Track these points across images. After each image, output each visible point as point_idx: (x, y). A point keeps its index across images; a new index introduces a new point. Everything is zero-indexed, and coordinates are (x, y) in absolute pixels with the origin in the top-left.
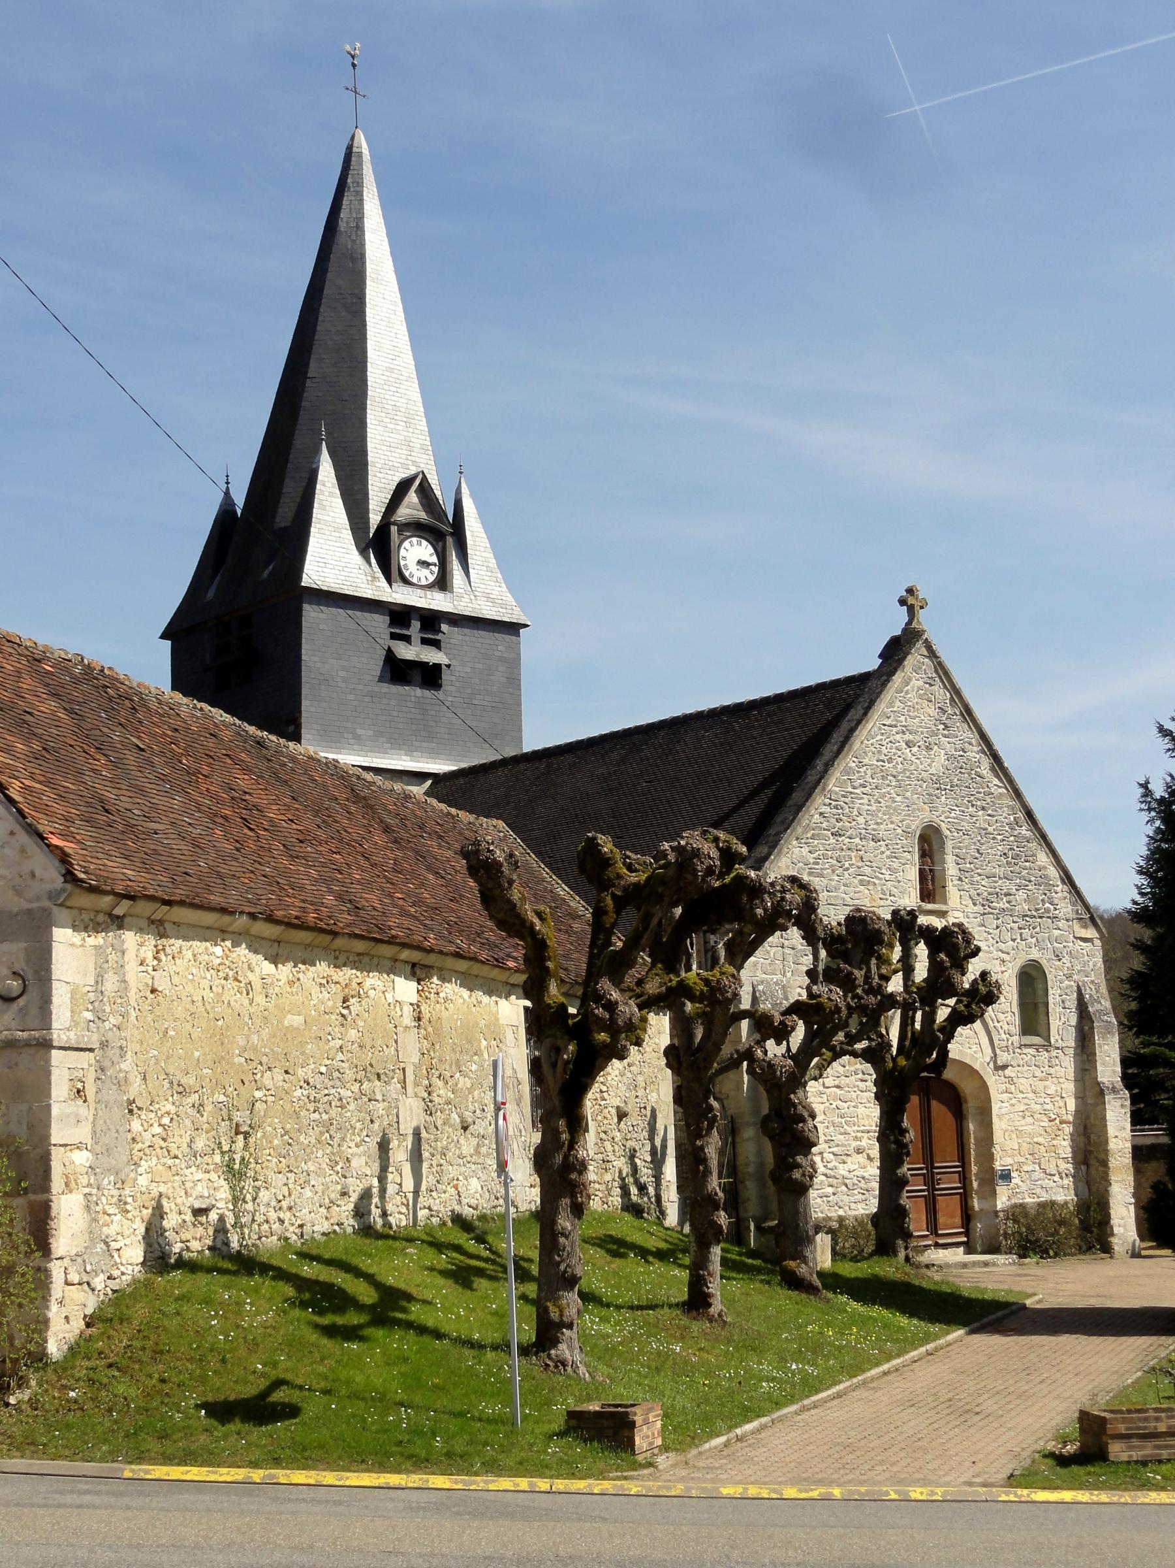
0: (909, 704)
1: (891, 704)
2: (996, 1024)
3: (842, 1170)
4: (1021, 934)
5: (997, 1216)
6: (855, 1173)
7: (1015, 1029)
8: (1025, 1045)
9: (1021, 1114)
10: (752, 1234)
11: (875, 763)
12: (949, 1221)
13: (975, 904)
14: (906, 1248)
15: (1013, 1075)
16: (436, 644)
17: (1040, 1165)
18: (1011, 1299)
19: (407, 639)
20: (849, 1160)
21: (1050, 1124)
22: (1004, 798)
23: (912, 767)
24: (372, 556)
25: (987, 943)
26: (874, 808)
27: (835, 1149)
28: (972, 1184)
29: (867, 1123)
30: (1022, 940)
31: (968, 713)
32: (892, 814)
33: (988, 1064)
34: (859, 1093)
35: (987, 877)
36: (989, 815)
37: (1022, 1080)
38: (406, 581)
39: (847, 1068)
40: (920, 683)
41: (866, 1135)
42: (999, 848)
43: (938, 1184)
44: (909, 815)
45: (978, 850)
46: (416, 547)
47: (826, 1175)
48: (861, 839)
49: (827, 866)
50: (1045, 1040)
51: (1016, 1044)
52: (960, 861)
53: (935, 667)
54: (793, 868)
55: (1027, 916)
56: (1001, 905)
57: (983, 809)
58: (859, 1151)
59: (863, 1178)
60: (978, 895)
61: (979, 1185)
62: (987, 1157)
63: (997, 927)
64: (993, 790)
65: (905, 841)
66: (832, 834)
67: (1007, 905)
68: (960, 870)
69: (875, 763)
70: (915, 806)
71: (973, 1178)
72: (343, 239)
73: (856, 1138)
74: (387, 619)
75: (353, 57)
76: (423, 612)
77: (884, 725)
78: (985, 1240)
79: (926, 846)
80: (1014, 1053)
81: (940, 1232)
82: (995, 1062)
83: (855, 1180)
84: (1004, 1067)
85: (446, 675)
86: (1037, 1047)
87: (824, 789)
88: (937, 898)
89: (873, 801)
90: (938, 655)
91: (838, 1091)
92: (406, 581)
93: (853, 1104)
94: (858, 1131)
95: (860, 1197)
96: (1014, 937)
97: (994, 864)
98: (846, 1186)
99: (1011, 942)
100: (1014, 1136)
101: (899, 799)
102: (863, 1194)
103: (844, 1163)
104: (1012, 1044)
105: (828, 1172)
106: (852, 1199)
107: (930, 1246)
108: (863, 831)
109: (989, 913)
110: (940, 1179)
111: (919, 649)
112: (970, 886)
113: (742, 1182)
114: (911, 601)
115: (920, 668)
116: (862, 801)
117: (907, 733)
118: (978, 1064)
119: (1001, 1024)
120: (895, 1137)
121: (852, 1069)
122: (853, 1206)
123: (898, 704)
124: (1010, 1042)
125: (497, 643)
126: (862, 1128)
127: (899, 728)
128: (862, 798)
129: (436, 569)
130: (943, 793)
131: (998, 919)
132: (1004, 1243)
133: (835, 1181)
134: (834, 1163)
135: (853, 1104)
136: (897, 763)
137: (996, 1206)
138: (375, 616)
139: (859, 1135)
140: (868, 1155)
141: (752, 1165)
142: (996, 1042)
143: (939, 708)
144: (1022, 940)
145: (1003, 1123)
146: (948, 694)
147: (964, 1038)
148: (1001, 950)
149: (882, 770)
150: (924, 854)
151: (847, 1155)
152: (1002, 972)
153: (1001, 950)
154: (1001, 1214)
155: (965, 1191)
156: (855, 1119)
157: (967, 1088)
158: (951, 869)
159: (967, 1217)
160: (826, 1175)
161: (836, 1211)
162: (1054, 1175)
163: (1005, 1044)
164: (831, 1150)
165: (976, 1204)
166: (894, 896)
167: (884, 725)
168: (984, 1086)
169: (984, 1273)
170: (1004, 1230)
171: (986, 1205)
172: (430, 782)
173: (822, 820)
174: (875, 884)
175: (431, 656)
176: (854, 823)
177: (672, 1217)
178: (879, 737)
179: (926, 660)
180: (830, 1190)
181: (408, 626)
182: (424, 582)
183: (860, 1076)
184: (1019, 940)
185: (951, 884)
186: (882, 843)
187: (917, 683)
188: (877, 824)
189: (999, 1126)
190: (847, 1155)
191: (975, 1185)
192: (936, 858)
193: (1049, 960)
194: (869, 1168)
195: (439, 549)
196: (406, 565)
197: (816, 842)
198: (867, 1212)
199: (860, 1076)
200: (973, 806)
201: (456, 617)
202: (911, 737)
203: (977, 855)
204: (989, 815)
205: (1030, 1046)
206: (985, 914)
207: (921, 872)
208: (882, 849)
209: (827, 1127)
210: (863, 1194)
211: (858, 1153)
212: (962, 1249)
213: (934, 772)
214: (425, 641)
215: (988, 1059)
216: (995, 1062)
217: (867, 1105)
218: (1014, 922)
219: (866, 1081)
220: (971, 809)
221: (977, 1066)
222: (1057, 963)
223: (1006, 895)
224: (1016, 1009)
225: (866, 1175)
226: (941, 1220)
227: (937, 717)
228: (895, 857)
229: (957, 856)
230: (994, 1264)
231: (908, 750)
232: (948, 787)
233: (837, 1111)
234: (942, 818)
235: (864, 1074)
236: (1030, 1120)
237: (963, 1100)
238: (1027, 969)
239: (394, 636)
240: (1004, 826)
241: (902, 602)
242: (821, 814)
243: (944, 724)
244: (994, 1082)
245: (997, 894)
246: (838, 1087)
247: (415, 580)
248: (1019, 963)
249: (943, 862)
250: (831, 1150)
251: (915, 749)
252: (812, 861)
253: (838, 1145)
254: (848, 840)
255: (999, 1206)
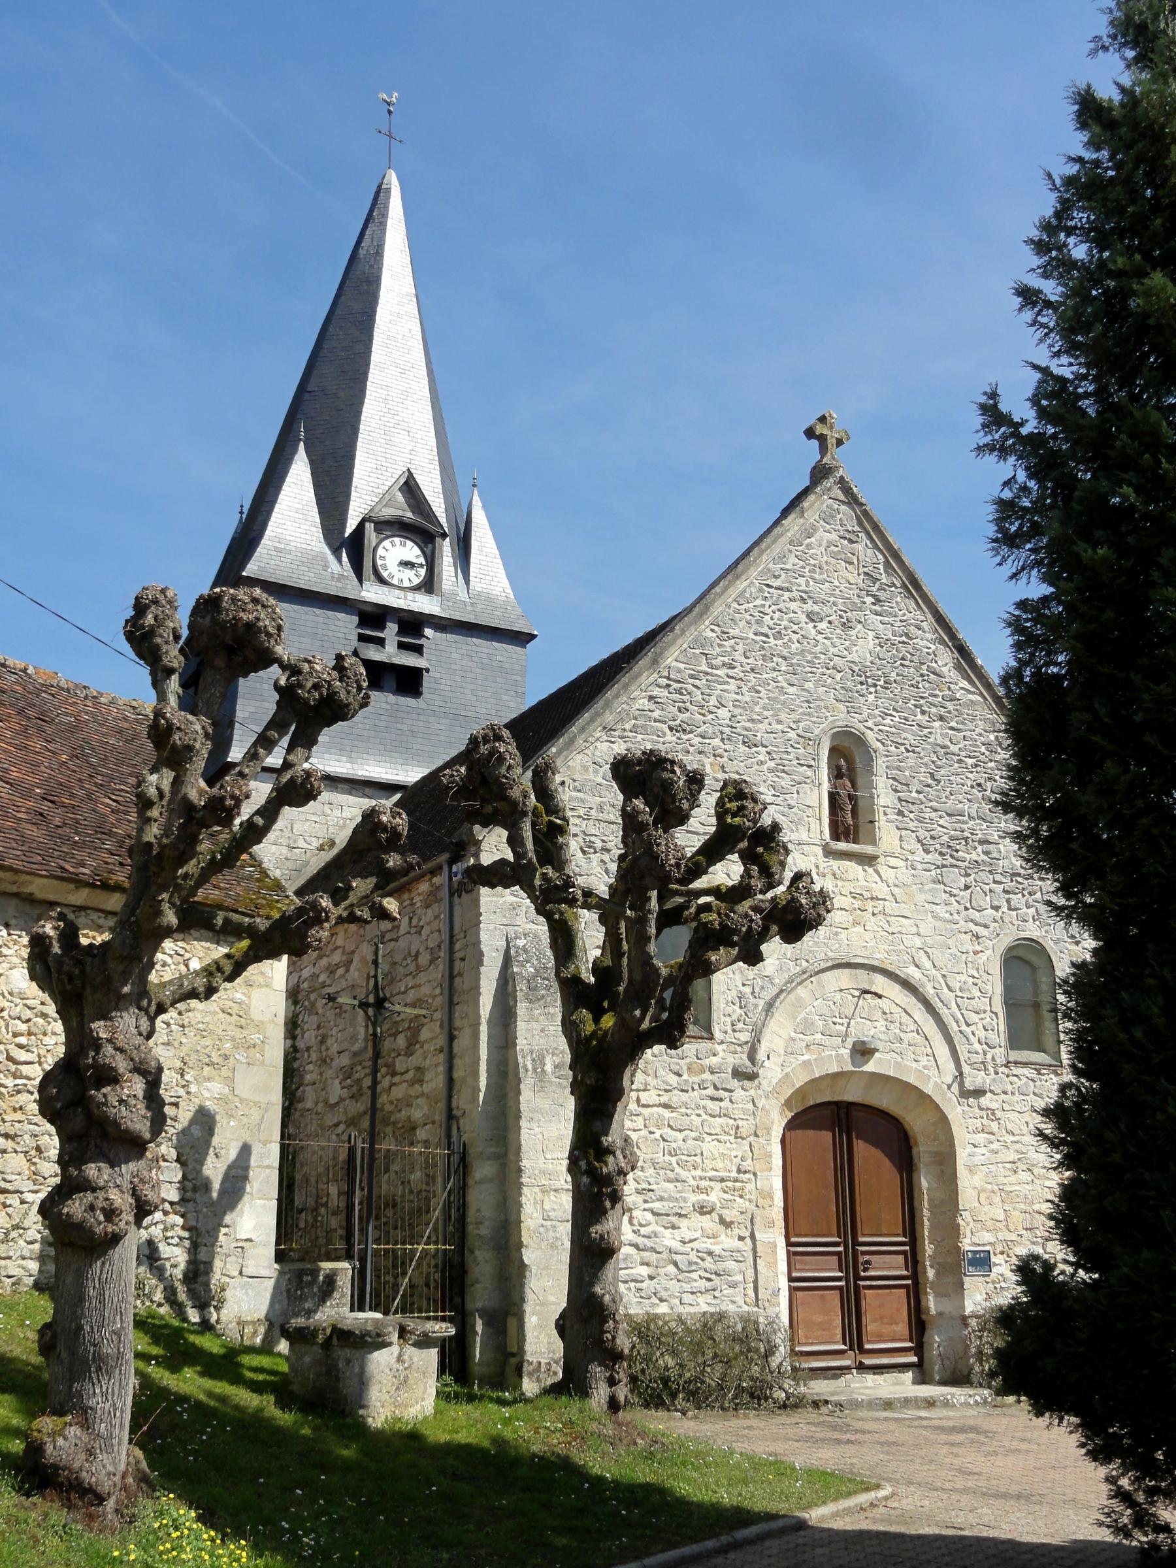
0: (812, 562)
1: (782, 558)
2: (964, 1028)
3: (669, 1239)
4: (1008, 901)
5: (966, 1325)
6: (695, 1245)
7: (1000, 1037)
8: (1016, 1063)
9: (1009, 1166)
10: (478, 1339)
11: (752, 636)
12: (886, 1330)
13: (927, 852)
14: (612, 1382)
15: (994, 1105)
16: (418, 650)
18: (759, 1499)
19: (381, 642)
20: (683, 1223)
22: (976, 707)
23: (818, 649)
24: (344, 555)
25: (948, 908)
26: (747, 699)
27: (657, 1205)
28: (925, 1272)
29: (720, 1165)
30: (1010, 909)
31: (913, 586)
33: (949, 1087)
34: (705, 1117)
35: (949, 815)
36: (952, 729)
37: (1011, 1115)
38: (382, 581)
39: (685, 1077)
40: (834, 536)
41: (718, 1186)
42: (970, 775)
43: (865, 1270)
44: (809, 714)
45: (932, 775)
46: (399, 548)
47: (636, 1246)
48: (722, 740)
50: (1054, 1058)
51: (1000, 1060)
52: (899, 787)
53: (858, 517)
54: (596, 771)
55: (1019, 875)
56: (974, 856)
57: (941, 718)
58: (703, 1210)
59: (710, 1253)
60: (933, 838)
61: (937, 1274)
62: (950, 1230)
63: (967, 887)
64: (958, 695)
65: (802, 751)
66: (671, 729)
67: (985, 858)
68: (900, 800)
69: (752, 636)
70: (822, 703)
71: (928, 1263)
72: (362, 267)
73: (698, 1189)
74: (356, 619)
75: (389, 104)
76: (402, 615)
77: (768, 586)
78: (946, 1362)
79: (842, 762)
80: (996, 1073)
81: (867, 1346)
82: (961, 1085)
83: (693, 1257)
84: (979, 1093)
85: (426, 679)
86: (1038, 1068)
87: (655, 662)
88: (861, 836)
89: (745, 688)
90: (863, 500)
91: (666, 1113)
92: (382, 581)
93: (694, 1134)
94: (701, 1178)
95: (703, 1284)
96: (996, 903)
97: (961, 797)
98: (676, 1264)
99: (990, 911)
100: (997, 1199)
101: (792, 690)
102: (709, 1280)
103: (674, 1227)
104: (993, 1059)
105: (640, 1241)
106: (687, 1287)
107: (848, 1368)
108: (727, 730)
109: (952, 866)
110: (868, 1262)
111: (829, 489)
112: (916, 823)
113: (472, 1252)
114: (820, 429)
115: (833, 517)
116: (725, 687)
117: (810, 602)
118: (931, 1085)
119: (973, 1028)
120: (589, 1163)
121: (696, 1079)
122: (687, 1298)
123: (793, 559)
124: (989, 1057)
125: (496, 652)
126: (712, 1174)
127: (796, 594)
128: (725, 683)
129: (423, 572)
130: (872, 689)
131: (968, 875)
132: (977, 1368)
133: (655, 1256)
134: (654, 1227)
135: (694, 1134)
136: (790, 640)
137: (963, 1308)
138: (340, 615)
139: (704, 1184)
140: (721, 1217)
141: (487, 1223)
142: (963, 1056)
143: (866, 574)
144: (1010, 909)
145: (976, 1178)
146: (880, 557)
147: (905, 1045)
148: (972, 921)
149: (763, 648)
150: (837, 774)
151: (680, 1215)
152: (976, 953)
153: (972, 921)
154: (973, 1322)
155: (916, 1283)
156: (698, 1159)
157: (916, 1122)
158: (883, 795)
159: (919, 1325)
160: (636, 1246)
161: (653, 1305)
163: (980, 1058)
164: (647, 1206)
165: (932, 1303)
167: (768, 586)
168: (943, 1120)
169: (886, 1419)
170: (978, 1347)
171: (947, 1306)
172: (398, 796)
173: (653, 707)
175: (408, 660)
176: (710, 717)
178: (759, 602)
179: (843, 507)
180: (644, 1271)
181: (382, 628)
182: (406, 584)
183: (710, 1091)
184: (1005, 909)
185: (883, 818)
187: (825, 535)
188: (752, 721)
189: (968, 1184)
190: (680, 1215)
191: (931, 1273)
192: (860, 781)
193: (1058, 941)
194: (723, 1237)
195: (428, 552)
196: (384, 566)
197: (640, 737)
198: (712, 1310)
199: (710, 1091)
200: (923, 713)
201: (444, 622)
202: (816, 608)
203: (930, 781)
204: (952, 729)
205: (1025, 1064)
206: (944, 866)
207: (833, 797)
208: (761, 757)
210: (709, 1280)
211: (702, 1213)
212: (909, 1375)
213: (856, 659)
214: (402, 646)
215: (949, 1080)
216: (961, 1085)
217: (722, 1138)
218: (995, 882)
219: (721, 1100)
220: (919, 717)
221: (928, 1089)
222: (1074, 947)
223: (981, 842)
224: (999, 1008)
225: (716, 1249)
226: (871, 1326)
227: (861, 585)
228: (783, 771)
229: (894, 779)
230: (947, 1404)
231: (811, 625)
232: (881, 683)
233: (662, 1144)
234: (870, 724)
235: (716, 1088)
236: (1027, 1176)
237: (912, 1140)
238: (1020, 953)
239: (362, 638)
240: (977, 746)
241: (810, 433)
242: (651, 698)
243: (873, 596)
244: (958, 1114)
245: (966, 839)
246: (666, 1106)
247: (395, 582)
248: (1006, 941)
249: (871, 785)
250: (647, 1206)
251: (823, 625)
253: (661, 1199)
254: (700, 739)
255: (969, 1308)
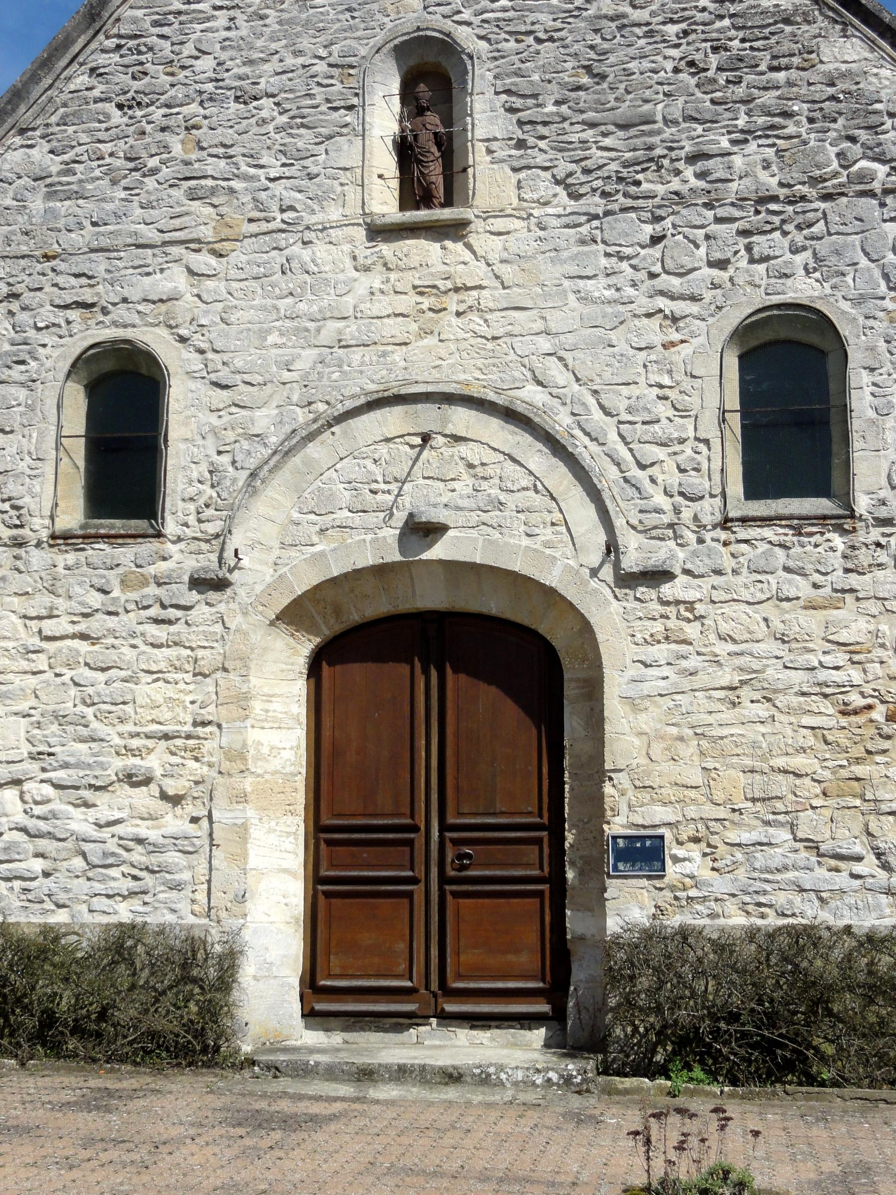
6: (119, 829)
17: (793, 827)
20: (101, 799)
21: (844, 721)
26: (244, 32)
27: (60, 775)
32: (298, 35)
33: (594, 572)
34: (143, 648)
49: (97, 173)
52: (518, 103)
68: (520, 123)
78: (585, 1016)
91: (83, 646)
102: (135, 878)
103: (87, 805)
108: (210, 87)
122: (100, 903)
156: (128, 709)
162: (859, 859)
166: (292, 208)
173: (94, 81)
174: (232, 191)
177: (322, 983)
180: (38, 865)
186: (264, 101)
188: (250, 62)
197: (71, 129)
209: (39, 725)
210: (135, 878)
215: (595, 558)
221: (551, 578)
223: (692, 159)
235: (164, 607)
246: (83, 637)
250: (45, 776)
252: (54, 169)
253: (66, 766)
